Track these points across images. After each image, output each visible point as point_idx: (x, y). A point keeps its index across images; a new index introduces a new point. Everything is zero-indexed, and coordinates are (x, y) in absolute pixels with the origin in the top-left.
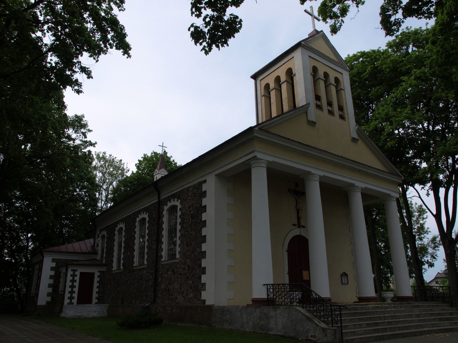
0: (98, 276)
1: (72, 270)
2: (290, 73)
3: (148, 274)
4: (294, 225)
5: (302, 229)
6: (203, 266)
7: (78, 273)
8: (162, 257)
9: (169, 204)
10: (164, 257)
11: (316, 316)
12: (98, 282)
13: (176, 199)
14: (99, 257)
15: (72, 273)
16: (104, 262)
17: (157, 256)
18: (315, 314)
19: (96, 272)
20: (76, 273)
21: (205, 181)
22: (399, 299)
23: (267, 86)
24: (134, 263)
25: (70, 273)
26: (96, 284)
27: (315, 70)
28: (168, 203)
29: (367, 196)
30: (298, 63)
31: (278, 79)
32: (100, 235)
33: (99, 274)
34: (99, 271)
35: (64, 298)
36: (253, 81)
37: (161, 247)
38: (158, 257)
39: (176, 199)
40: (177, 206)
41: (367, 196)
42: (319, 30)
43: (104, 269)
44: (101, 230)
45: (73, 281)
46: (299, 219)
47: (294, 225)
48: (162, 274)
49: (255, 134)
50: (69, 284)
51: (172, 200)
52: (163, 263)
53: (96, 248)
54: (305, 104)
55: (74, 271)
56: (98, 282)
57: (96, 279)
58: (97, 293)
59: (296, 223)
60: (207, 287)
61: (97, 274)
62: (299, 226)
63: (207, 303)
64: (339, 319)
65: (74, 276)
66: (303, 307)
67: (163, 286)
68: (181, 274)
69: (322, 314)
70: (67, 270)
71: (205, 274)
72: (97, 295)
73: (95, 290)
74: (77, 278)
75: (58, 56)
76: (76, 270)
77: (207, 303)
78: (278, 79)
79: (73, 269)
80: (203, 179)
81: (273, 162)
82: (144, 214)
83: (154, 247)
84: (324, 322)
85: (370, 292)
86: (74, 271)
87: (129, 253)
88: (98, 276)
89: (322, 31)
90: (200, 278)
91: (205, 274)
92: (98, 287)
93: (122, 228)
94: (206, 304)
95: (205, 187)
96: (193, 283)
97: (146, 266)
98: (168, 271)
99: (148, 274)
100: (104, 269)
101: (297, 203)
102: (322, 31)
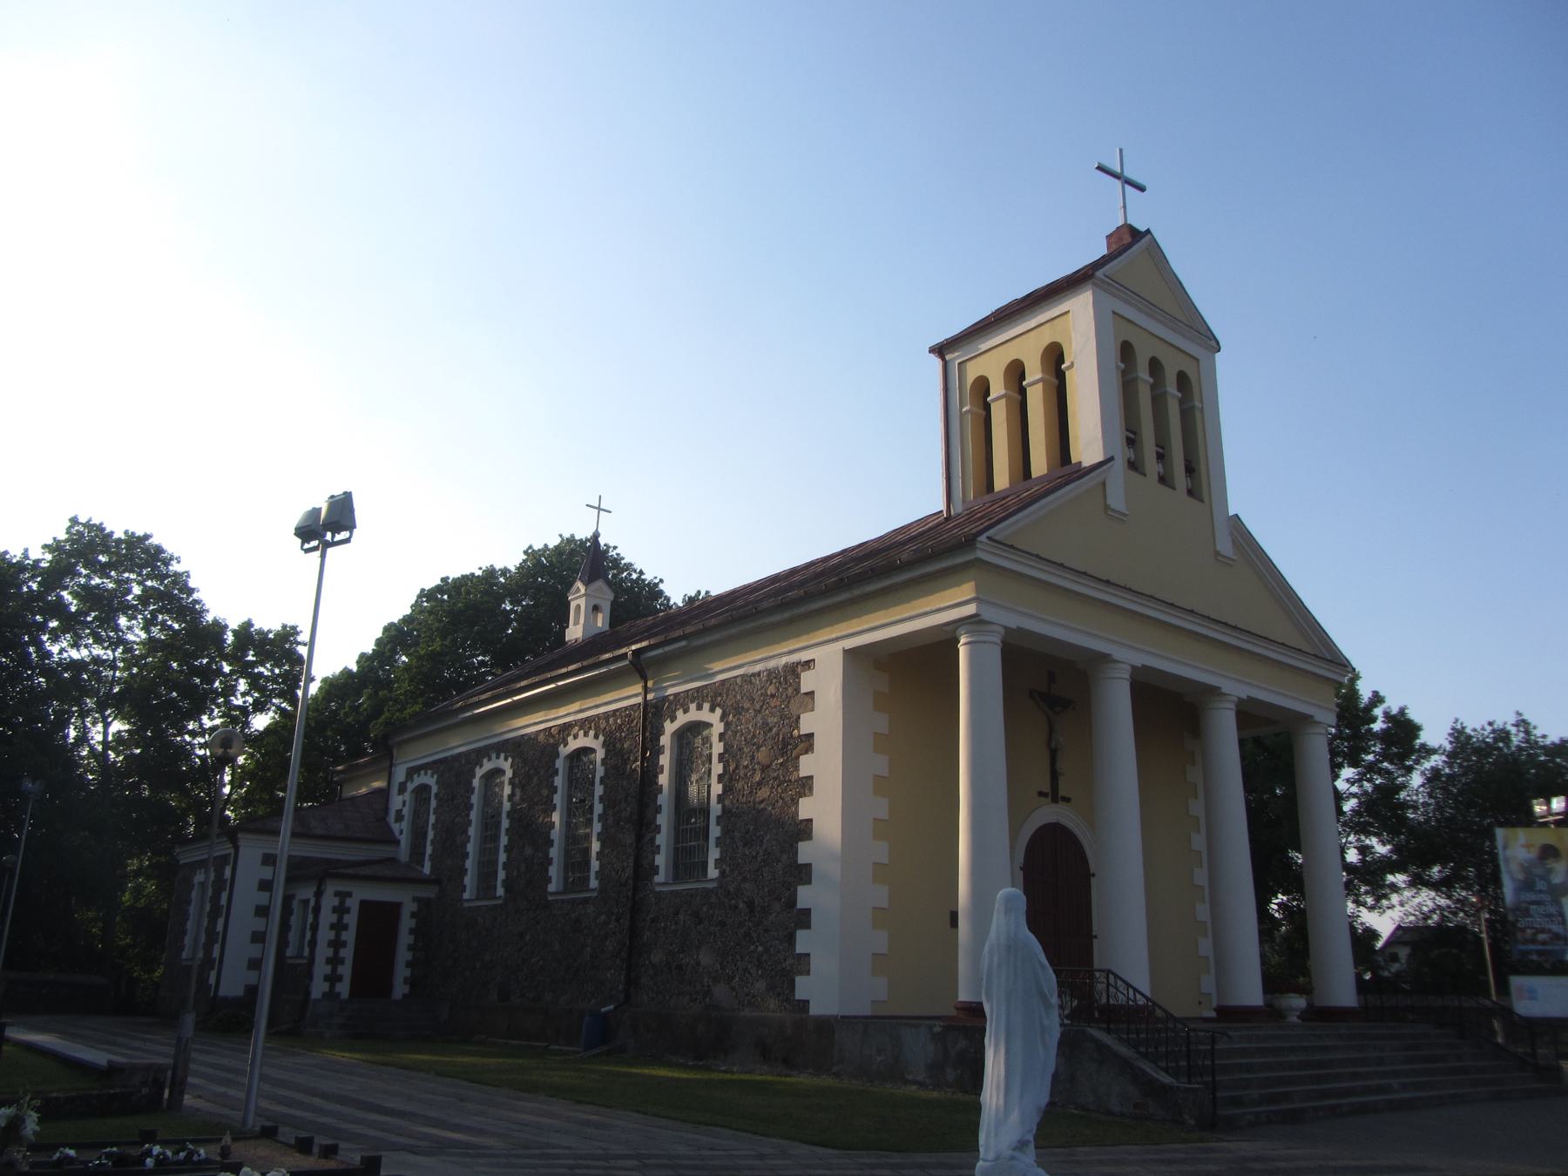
0: (413, 915)
1: (337, 894)
2: (1055, 357)
3: (603, 918)
4: (1041, 794)
5: (1061, 805)
6: (800, 905)
7: (353, 904)
8: (655, 870)
9: (682, 719)
10: (662, 870)
11: (1145, 1056)
12: (411, 931)
13: (706, 706)
14: (403, 852)
15: (336, 901)
16: (427, 869)
17: (637, 865)
18: (1142, 1049)
19: (405, 897)
20: (349, 902)
21: (808, 664)
22: (1321, 1015)
23: (982, 386)
24: (549, 880)
25: (329, 901)
26: (405, 939)
27: (1126, 350)
28: (680, 713)
29: (1249, 714)
30: (1078, 325)
31: (1016, 372)
32: (410, 786)
33: (414, 907)
34: (415, 899)
35: (310, 976)
36: (936, 362)
37: (653, 840)
38: (643, 871)
39: (706, 706)
40: (709, 725)
41: (1249, 714)
42: (1143, 229)
43: (430, 892)
44: (411, 772)
45: (339, 927)
46: (1055, 776)
47: (1041, 794)
48: (653, 921)
49: (980, 555)
50: (325, 934)
51: (693, 706)
52: (658, 889)
53: (396, 827)
54: (1099, 458)
55: (343, 896)
56: (411, 931)
57: (407, 923)
58: (409, 964)
59: (1047, 788)
60: (814, 964)
61: (409, 907)
62: (1055, 797)
63: (815, 1010)
64: (1208, 1063)
65: (341, 910)
66: (1109, 1031)
67: (657, 957)
68: (722, 924)
69: (1162, 1049)
70: (319, 894)
71: (809, 927)
72: (408, 972)
73: (403, 955)
74: (352, 919)
75: (1435, 864)
76: (350, 894)
77: (815, 1010)
78: (1016, 372)
79: (418, 894)
80: (804, 656)
81: (1020, 631)
82: (586, 734)
83: (629, 839)
84: (1166, 1070)
85: (1250, 992)
86: (343, 896)
87: (528, 851)
88: (413, 915)
89: (1148, 231)
90: (791, 939)
91: (809, 927)
92: (410, 948)
93: (499, 772)
94: (811, 1013)
95: (807, 681)
96: (767, 950)
97: (594, 894)
98: (677, 913)
99: (603, 918)
100: (430, 892)
101: (1051, 731)
102: (1148, 231)
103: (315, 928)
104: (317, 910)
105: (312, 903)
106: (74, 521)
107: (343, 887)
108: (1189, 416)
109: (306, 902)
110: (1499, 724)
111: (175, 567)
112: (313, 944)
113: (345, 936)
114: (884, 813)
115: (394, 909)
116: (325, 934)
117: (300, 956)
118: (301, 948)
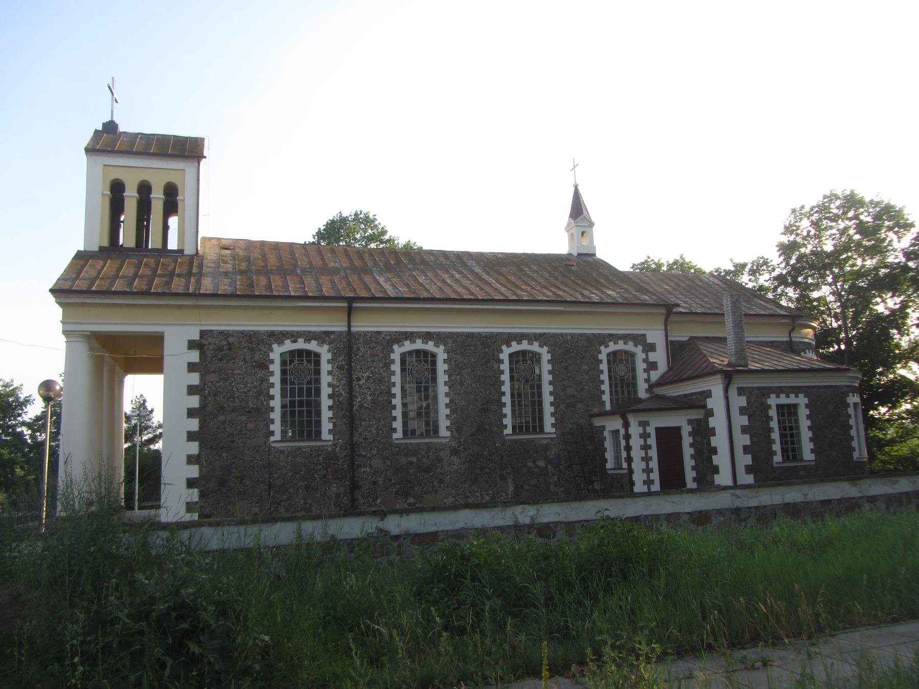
7: (651, 430)
19: (680, 420)
20: (648, 430)
25: (635, 430)
33: (690, 429)
55: (644, 424)
57: (687, 440)
61: (686, 430)
65: (645, 436)
70: (626, 425)
74: (652, 441)
103: (628, 448)
104: (627, 437)
105: (622, 432)
106: (203, 139)
107: (644, 417)
108: (454, 284)
109: (616, 433)
110: (344, 215)
111: (100, 128)
112: (629, 460)
113: (652, 476)
114: (807, 402)
115: (676, 432)
116: (637, 454)
117: (618, 466)
118: (617, 457)
